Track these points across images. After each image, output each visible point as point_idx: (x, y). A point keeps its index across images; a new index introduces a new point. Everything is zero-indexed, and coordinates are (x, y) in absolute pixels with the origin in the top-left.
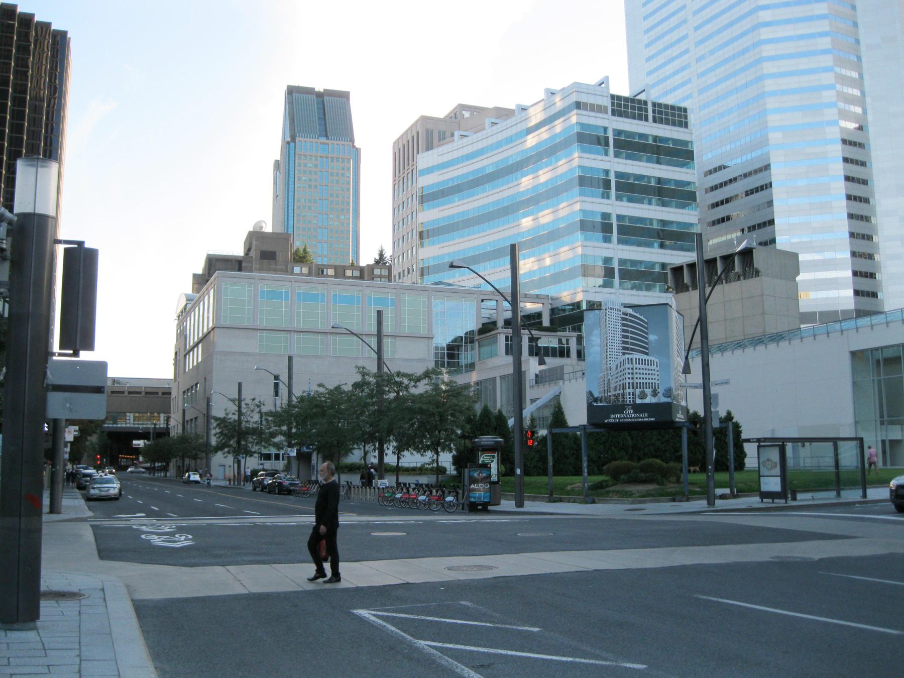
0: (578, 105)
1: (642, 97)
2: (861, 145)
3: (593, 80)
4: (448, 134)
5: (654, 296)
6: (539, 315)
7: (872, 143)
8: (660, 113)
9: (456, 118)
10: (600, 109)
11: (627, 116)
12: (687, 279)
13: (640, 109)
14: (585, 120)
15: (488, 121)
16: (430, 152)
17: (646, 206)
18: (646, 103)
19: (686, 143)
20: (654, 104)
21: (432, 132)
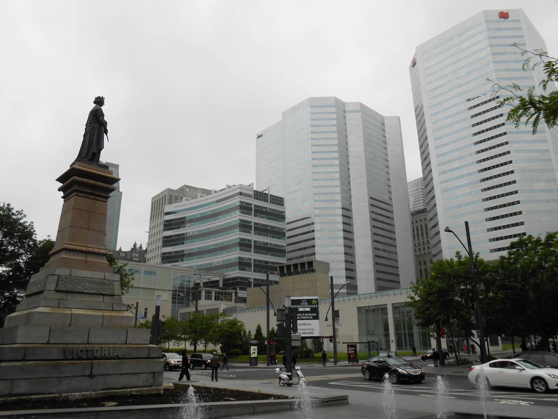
0: (241, 194)
1: (266, 192)
4: (179, 198)
6: (218, 282)
9: (183, 190)
10: (249, 196)
11: (260, 200)
12: (285, 272)
14: (243, 200)
15: (199, 195)
16: (171, 205)
18: (268, 194)
20: (271, 195)
21: (172, 196)
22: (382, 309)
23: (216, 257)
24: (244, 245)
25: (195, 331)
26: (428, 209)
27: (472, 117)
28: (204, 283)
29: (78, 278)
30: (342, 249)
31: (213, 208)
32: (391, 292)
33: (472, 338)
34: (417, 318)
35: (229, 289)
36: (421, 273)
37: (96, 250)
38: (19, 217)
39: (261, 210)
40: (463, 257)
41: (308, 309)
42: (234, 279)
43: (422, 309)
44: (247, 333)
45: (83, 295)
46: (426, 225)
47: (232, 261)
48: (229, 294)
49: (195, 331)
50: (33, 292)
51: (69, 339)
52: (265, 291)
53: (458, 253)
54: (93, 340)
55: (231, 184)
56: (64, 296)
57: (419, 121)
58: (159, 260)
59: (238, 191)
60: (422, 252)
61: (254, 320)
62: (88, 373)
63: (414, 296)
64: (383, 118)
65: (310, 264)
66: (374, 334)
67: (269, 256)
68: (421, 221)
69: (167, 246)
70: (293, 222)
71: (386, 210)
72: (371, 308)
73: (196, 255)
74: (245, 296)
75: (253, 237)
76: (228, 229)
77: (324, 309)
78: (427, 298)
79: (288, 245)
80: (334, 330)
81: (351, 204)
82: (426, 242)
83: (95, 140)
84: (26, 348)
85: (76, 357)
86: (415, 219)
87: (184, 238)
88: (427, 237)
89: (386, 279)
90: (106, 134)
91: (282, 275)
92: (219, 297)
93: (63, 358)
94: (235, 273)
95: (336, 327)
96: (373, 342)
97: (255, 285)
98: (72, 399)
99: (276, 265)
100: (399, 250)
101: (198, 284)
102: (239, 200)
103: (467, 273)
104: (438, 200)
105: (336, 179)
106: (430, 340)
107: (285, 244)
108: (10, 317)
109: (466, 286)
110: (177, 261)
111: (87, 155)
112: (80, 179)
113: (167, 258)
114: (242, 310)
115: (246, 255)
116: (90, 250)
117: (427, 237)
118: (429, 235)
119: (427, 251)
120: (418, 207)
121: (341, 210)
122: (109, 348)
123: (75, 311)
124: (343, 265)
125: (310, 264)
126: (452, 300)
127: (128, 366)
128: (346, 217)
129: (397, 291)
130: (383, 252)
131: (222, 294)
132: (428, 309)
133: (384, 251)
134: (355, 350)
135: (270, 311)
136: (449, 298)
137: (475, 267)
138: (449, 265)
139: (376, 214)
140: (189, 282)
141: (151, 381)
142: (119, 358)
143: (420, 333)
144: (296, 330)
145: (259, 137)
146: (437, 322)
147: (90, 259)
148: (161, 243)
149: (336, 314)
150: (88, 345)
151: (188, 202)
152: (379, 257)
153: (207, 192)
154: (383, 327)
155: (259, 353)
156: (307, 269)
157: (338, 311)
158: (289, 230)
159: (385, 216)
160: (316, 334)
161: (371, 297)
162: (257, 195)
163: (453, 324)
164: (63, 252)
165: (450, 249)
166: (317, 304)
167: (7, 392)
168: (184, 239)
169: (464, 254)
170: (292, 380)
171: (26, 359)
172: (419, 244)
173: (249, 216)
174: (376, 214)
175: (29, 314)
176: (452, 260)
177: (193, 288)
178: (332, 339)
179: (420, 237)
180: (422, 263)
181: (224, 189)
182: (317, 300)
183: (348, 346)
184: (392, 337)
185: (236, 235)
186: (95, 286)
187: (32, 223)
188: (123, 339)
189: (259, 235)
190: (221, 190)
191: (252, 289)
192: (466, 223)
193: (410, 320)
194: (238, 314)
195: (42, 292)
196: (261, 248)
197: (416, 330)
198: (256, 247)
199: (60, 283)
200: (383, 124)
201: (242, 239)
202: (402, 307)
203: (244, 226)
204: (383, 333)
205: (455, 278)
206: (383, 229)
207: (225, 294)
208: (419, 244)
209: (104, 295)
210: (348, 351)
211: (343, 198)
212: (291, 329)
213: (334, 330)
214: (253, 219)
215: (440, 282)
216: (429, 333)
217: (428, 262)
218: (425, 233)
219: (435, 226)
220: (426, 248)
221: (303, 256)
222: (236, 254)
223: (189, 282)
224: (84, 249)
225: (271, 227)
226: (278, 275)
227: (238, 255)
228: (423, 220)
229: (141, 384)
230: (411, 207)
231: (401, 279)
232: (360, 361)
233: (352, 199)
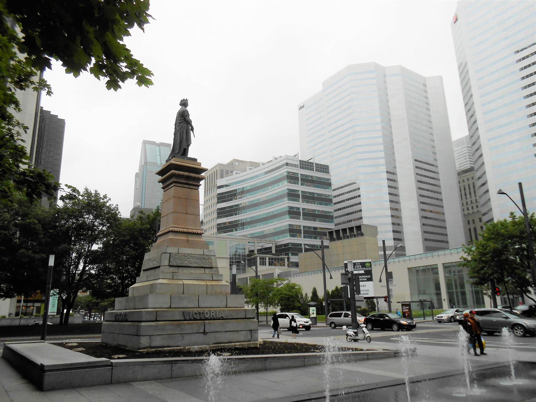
0: (287, 164)
2: (394, 174)
3: (292, 154)
4: (229, 172)
5: (461, 268)
6: (270, 248)
7: (398, 180)
8: (318, 167)
10: (295, 166)
11: (306, 169)
13: (311, 166)
14: (290, 170)
15: (248, 168)
17: (313, 205)
19: (328, 179)
22: (432, 269)
23: (267, 225)
24: (293, 213)
25: (257, 295)
26: (476, 167)
27: (522, 69)
28: (258, 250)
29: (185, 255)
30: (389, 212)
31: (261, 180)
32: (441, 253)
33: (528, 294)
34: (471, 277)
35: (281, 255)
36: (471, 234)
37: (195, 231)
38: (105, 200)
39: (308, 180)
40: (517, 217)
41: (362, 272)
42: (286, 245)
43: (477, 268)
44: (304, 295)
45: (189, 269)
46: (473, 183)
47: (283, 229)
48: (281, 259)
49: (257, 295)
50: (150, 267)
51: (185, 304)
52: (321, 255)
53: (512, 214)
54: (202, 305)
55: (277, 156)
56: (175, 270)
57: (462, 72)
58: (215, 230)
59: (285, 162)
60: (471, 211)
61: (310, 283)
62: (202, 331)
63: (467, 257)
64: (424, 79)
65: (359, 228)
66: (425, 294)
67: (317, 222)
68: (468, 180)
69: (221, 217)
70: (339, 188)
71: (431, 171)
72: (421, 268)
73: (248, 224)
74: (297, 261)
75: (301, 205)
76: (277, 198)
77: (377, 270)
78: (480, 258)
79: (335, 211)
80: (389, 291)
81: (395, 167)
82: (474, 201)
83: (184, 137)
84: (157, 312)
85: (192, 319)
86: (462, 179)
87: (237, 209)
88: (475, 196)
89: (435, 239)
90: (193, 131)
91: (332, 239)
92: (272, 262)
93: (183, 319)
94: (287, 239)
95: (390, 287)
96: (425, 301)
97: (306, 250)
98: (193, 351)
99: (325, 231)
100: (446, 210)
101: (253, 251)
102: (286, 170)
103: (522, 232)
104: (486, 159)
105: (380, 144)
106: (483, 298)
107: (332, 211)
108: (134, 287)
109: (521, 245)
110: (232, 231)
111: (180, 150)
112: (177, 172)
113: (222, 228)
114: (295, 274)
115: (295, 222)
116: (190, 231)
117: (475, 196)
118: (477, 194)
119: (475, 210)
120: (464, 165)
121: (386, 174)
122: (216, 311)
123: (186, 282)
124: (390, 228)
125: (359, 228)
126: (507, 259)
127: (231, 325)
128: (391, 180)
129: (447, 252)
130: (430, 213)
131: (275, 259)
132: (482, 268)
133: (431, 212)
134: (410, 309)
135: (326, 273)
136: (504, 257)
137: (530, 227)
138: (502, 225)
139: (421, 175)
140: (244, 249)
141: (249, 337)
142: (223, 319)
143: (472, 292)
144: (359, 292)
145: (301, 108)
146: (492, 281)
147: (191, 238)
148: (215, 215)
149: (389, 276)
150: (199, 309)
151: (238, 175)
152: (426, 218)
153: (255, 165)
154: (434, 287)
155: (318, 314)
156: (355, 233)
157: (391, 273)
158: (335, 197)
159: (431, 178)
160: (371, 295)
161: (421, 258)
162: (303, 164)
163: (507, 282)
164: (170, 234)
165: (502, 211)
166: (371, 266)
167: (148, 345)
168: (237, 209)
169: (519, 214)
170: (357, 336)
171: (158, 319)
172: (467, 203)
173: (297, 185)
174: (421, 175)
175: (152, 285)
176: (505, 221)
177: (248, 256)
178: (387, 299)
179: (468, 196)
180: (471, 222)
181: (272, 161)
182: (370, 262)
183: (403, 305)
184: (444, 295)
185: (286, 204)
186: (197, 260)
187: (117, 205)
188: (224, 304)
189: (307, 203)
190: (268, 162)
191: (303, 254)
192: (520, 184)
193: (461, 278)
194: (292, 278)
195: (159, 267)
196: (310, 215)
197: (468, 289)
198: (304, 214)
199: (171, 259)
200: (425, 85)
201: (291, 208)
202: (453, 266)
203: (292, 195)
204: (435, 292)
205: (509, 238)
206: (428, 190)
207: (278, 259)
208: (467, 203)
209: (204, 268)
210: (403, 310)
211: (388, 164)
212: (354, 291)
213: (389, 291)
214: (300, 188)
215: (494, 243)
216: (482, 292)
217: (477, 220)
218: (472, 192)
219: (484, 184)
220: (475, 207)
221: (350, 221)
222: (286, 222)
223: (244, 249)
224: (185, 230)
225: (318, 194)
226: (328, 239)
227: (287, 223)
228: (470, 179)
229: (242, 340)
230: (457, 166)
231: (450, 239)
232: (414, 319)
233: (397, 163)
